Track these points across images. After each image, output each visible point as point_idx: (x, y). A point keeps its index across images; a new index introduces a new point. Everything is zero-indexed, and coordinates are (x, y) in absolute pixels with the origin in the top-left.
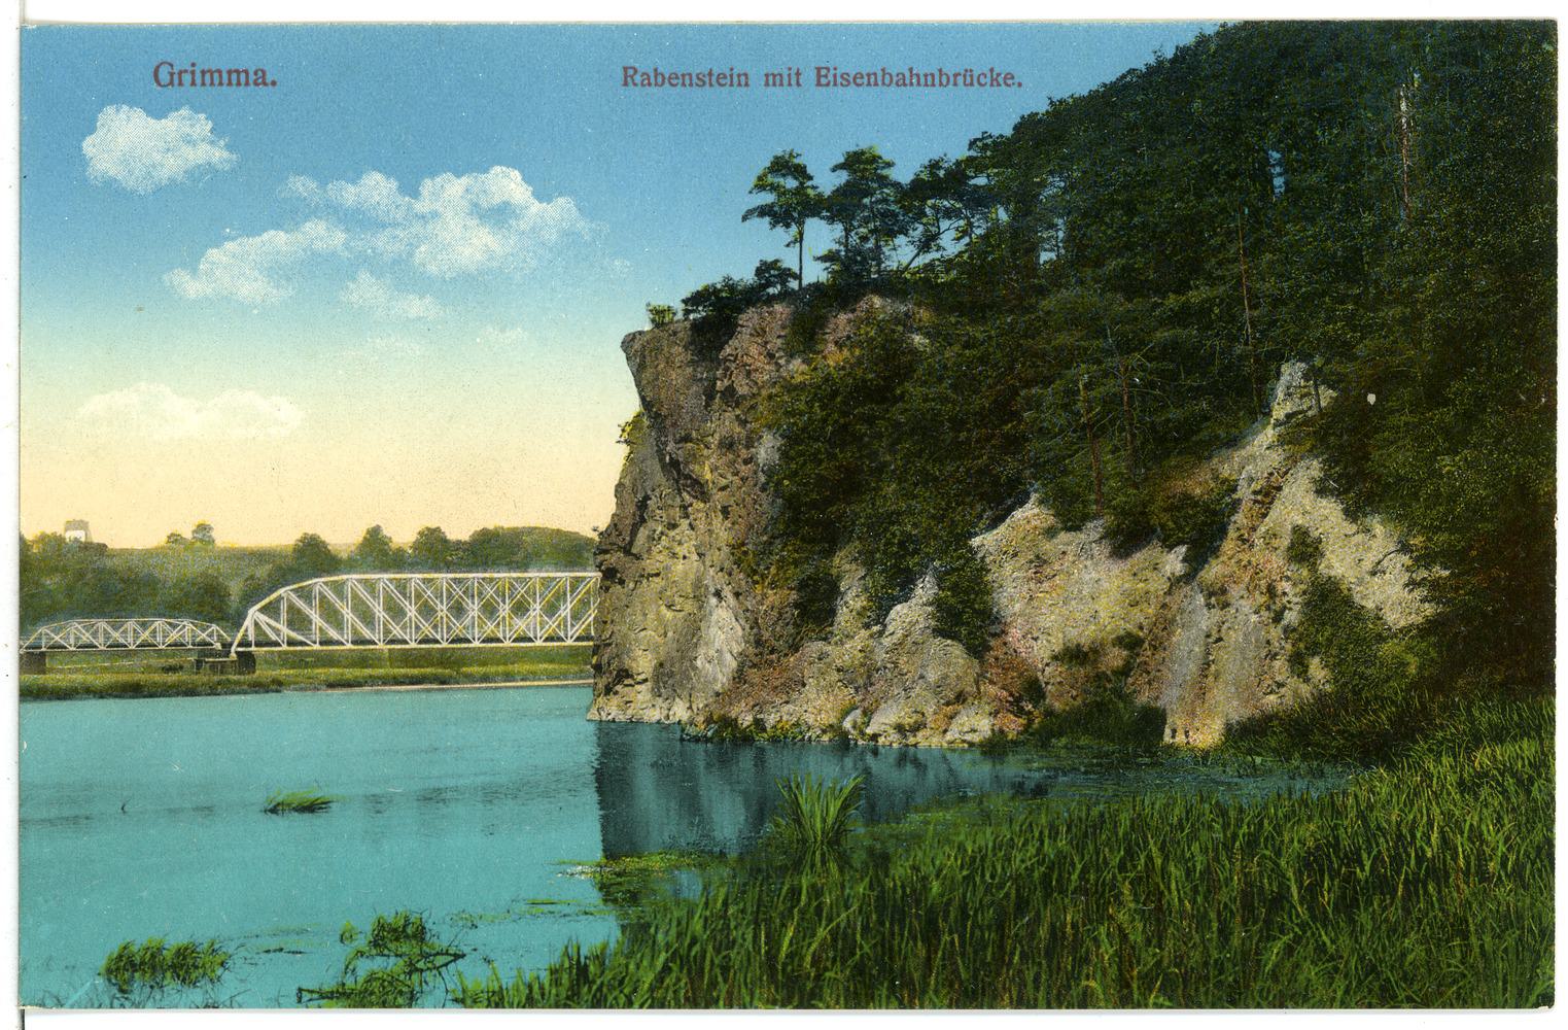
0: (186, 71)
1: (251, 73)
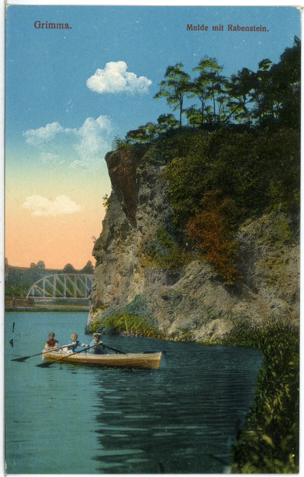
0: (44, 24)
1: (249, 28)
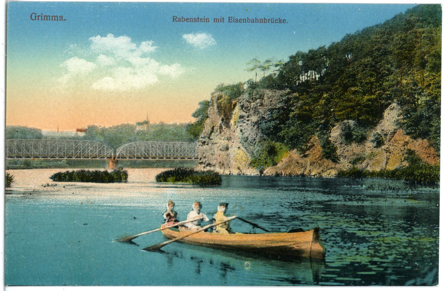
0: (40, 16)
